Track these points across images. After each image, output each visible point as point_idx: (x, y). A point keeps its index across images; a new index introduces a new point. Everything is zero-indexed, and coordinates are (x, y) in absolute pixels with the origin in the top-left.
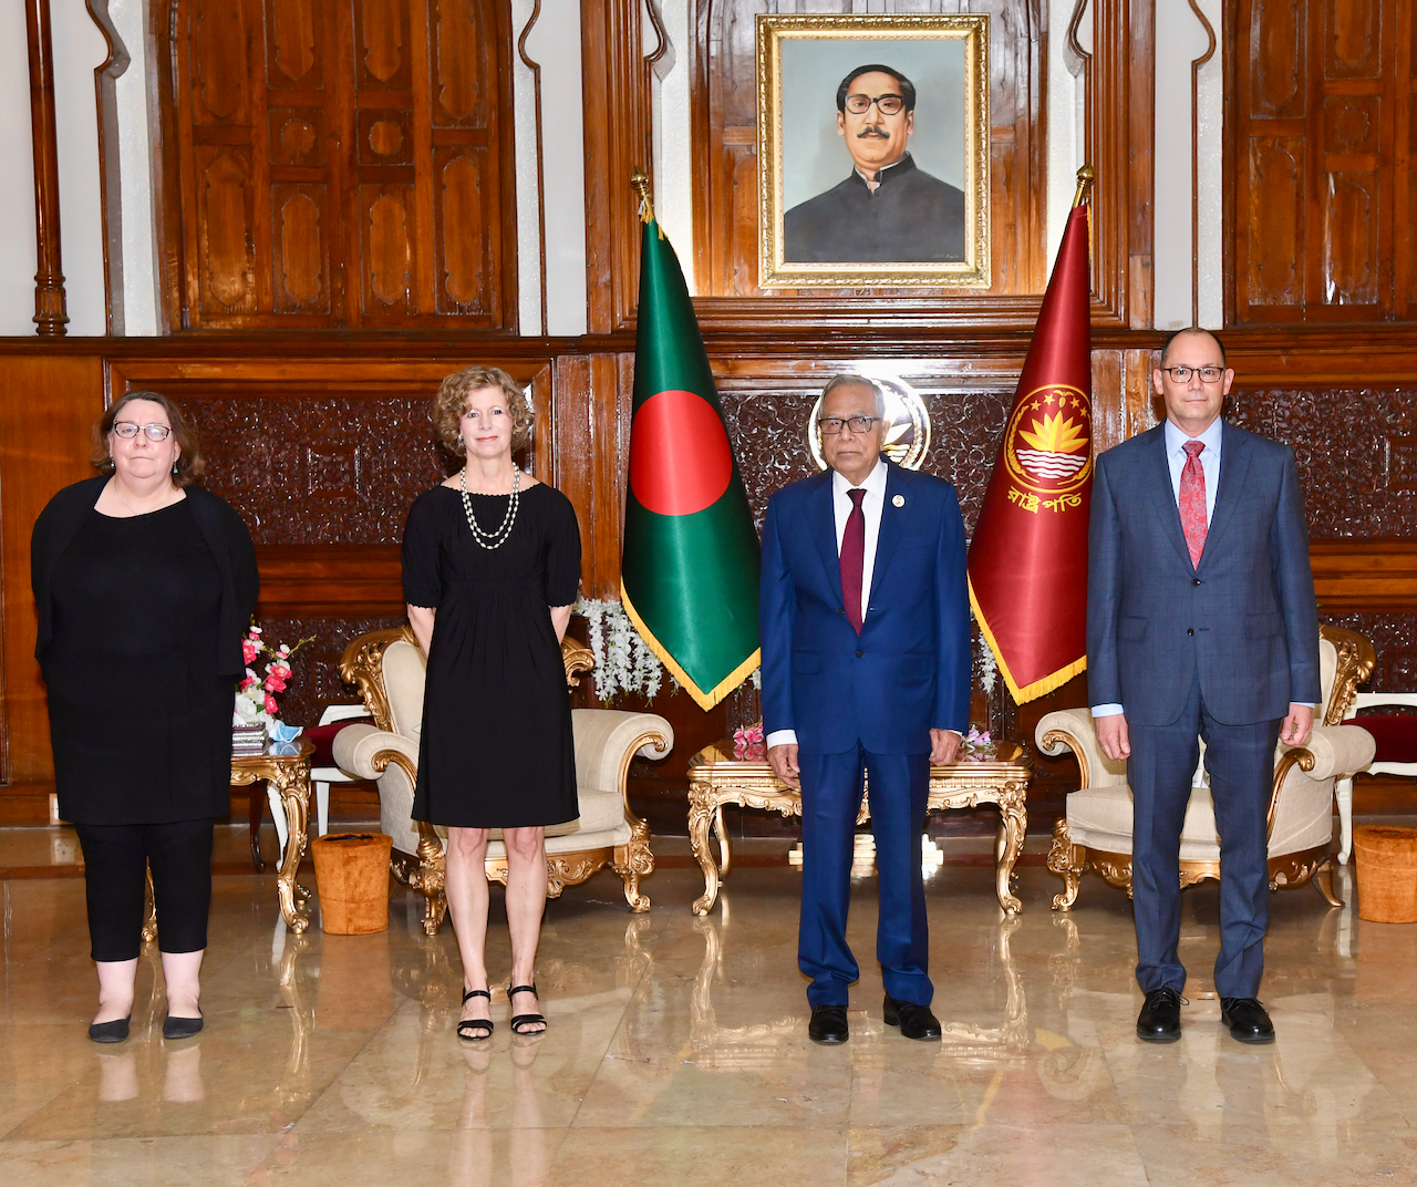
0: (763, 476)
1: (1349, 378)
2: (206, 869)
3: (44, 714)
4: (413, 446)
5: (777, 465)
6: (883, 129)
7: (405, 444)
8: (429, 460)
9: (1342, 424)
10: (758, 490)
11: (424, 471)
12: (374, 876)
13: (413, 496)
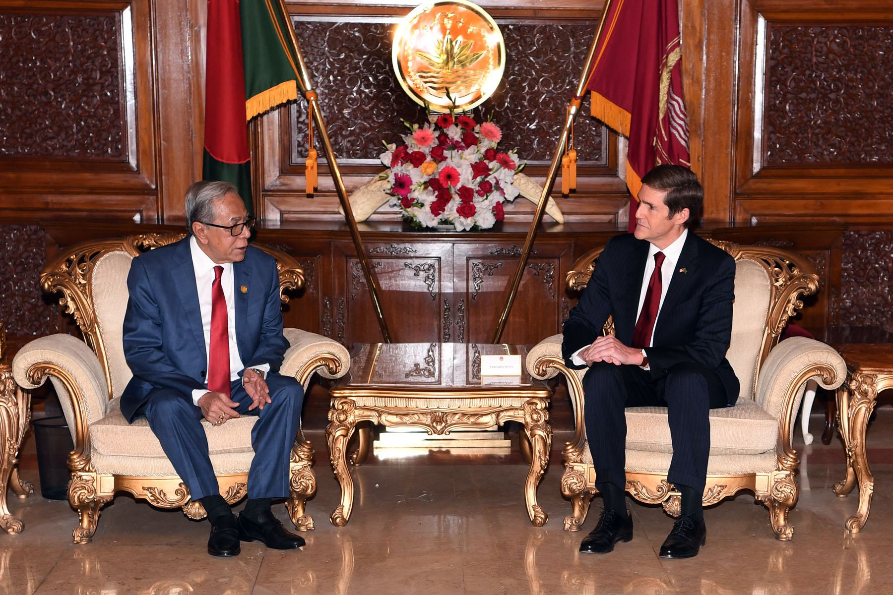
0: (350, 99)
1: (881, 16)
2: (467, 336)
3: (216, 474)
4: (18, 62)
5: (363, 88)
7: (10, 59)
8: (34, 75)
9: (873, 58)
10: (346, 111)
11: (30, 86)
12: (309, 162)
13: (20, 110)
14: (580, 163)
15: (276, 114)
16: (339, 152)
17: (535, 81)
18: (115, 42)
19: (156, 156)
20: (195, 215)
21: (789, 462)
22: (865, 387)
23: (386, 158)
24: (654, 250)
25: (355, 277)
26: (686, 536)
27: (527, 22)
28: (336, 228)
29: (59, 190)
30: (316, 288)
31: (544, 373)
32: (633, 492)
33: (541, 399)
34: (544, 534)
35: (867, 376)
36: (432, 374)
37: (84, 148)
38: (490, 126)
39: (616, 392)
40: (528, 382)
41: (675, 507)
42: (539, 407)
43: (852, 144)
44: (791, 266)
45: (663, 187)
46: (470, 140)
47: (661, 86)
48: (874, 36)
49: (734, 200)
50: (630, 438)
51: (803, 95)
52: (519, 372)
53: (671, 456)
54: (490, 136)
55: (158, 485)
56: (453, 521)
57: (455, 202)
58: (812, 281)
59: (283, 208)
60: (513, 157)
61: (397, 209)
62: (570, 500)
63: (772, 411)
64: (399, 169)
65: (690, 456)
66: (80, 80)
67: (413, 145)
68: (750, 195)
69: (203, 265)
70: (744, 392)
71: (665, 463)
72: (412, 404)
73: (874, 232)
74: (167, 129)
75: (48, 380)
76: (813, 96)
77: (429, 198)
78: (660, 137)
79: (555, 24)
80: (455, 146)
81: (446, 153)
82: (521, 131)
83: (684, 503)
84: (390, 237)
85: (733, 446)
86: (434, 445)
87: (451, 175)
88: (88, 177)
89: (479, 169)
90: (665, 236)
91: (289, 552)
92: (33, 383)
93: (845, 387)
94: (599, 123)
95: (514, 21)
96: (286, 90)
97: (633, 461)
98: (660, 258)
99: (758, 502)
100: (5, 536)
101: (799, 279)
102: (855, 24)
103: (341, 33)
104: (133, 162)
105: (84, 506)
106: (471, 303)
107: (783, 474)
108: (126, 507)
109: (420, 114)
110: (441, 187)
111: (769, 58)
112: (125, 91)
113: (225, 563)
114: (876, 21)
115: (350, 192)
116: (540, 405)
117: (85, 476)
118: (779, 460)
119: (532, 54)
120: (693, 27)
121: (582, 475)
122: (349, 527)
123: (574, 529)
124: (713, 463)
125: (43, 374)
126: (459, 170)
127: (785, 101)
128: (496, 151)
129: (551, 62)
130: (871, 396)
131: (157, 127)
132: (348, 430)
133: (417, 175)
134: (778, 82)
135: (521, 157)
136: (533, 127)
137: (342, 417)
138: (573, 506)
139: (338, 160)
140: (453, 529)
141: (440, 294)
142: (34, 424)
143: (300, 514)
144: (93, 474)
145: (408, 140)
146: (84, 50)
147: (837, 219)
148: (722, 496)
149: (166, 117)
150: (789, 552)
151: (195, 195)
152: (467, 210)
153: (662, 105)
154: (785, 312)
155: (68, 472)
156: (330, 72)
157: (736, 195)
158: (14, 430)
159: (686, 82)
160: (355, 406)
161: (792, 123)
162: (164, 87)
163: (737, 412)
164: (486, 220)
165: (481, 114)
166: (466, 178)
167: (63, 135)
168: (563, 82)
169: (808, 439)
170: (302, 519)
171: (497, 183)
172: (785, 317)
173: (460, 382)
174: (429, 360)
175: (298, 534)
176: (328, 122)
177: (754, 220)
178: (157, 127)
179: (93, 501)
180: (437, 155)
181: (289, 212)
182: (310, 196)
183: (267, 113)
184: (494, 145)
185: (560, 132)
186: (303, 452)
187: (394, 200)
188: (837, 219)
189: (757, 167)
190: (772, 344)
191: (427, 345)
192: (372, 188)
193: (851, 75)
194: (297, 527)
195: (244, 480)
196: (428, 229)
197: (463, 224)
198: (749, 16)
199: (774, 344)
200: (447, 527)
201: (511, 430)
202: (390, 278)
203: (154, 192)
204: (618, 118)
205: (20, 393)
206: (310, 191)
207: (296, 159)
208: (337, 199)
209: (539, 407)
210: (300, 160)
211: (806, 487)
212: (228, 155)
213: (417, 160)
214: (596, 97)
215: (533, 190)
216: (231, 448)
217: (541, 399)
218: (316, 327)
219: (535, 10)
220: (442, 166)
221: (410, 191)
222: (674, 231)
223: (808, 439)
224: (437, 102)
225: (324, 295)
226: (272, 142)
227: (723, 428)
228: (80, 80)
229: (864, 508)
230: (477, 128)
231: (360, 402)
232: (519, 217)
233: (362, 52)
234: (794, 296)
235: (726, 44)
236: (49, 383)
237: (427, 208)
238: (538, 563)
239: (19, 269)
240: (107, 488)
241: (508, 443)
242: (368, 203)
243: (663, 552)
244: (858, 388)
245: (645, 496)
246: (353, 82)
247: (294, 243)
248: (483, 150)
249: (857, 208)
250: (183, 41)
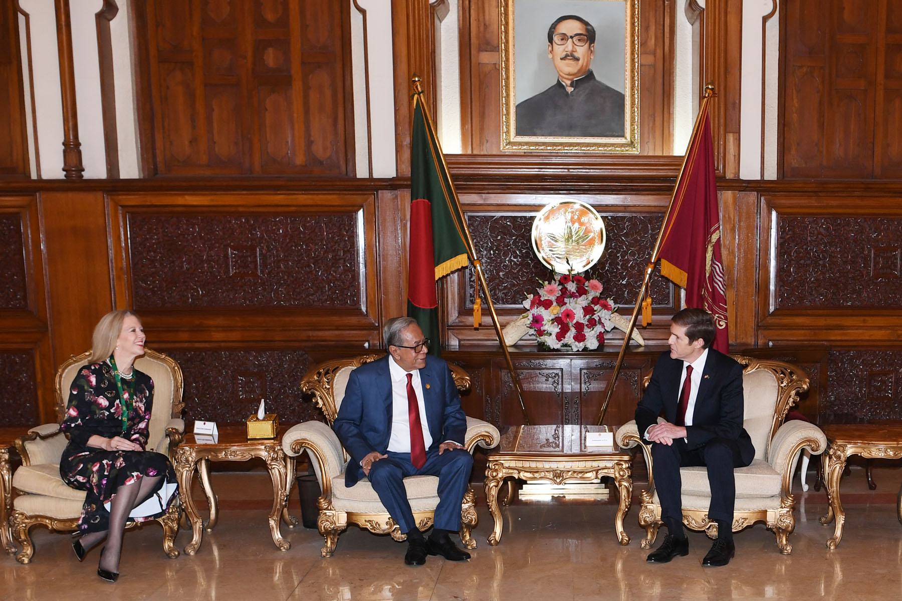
6: (576, 54)
12: (475, 307)
14: (655, 306)
15: (456, 275)
16: (496, 300)
17: (626, 253)
18: (353, 232)
19: (378, 304)
20: (391, 341)
21: (789, 502)
22: (839, 453)
23: (527, 304)
24: (686, 364)
25: (506, 382)
26: (722, 549)
27: (620, 214)
28: (494, 350)
29: (315, 328)
30: (481, 389)
31: (628, 444)
32: (686, 522)
33: (626, 461)
34: (628, 550)
35: (840, 446)
36: (558, 446)
37: (332, 300)
38: (595, 282)
39: (684, 454)
40: (619, 451)
41: (714, 533)
42: (624, 466)
43: (834, 293)
44: (791, 373)
45: (685, 324)
46: (581, 291)
47: (707, 255)
48: (848, 224)
49: (757, 331)
50: (684, 487)
51: (802, 262)
52: (611, 443)
53: (710, 499)
54: (595, 288)
55: (375, 519)
56: (572, 542)
57: (572, 332)
58: (805, 383)
59: (460, 337)
60: (611, 302)
61: (534, 337)
62: (645, 528)
63: (778, 470)
64: (536, 311)
65: (723, 499)
67: (544, 294)
68: (767, 327)
69: (397, 373)
70: (759, 455)
71: (706, 503)
72: (540, 465)
73: (849, 351)
74: (386, 288)
75: (305, 451)
76: (809, 262)
77: (555, 329)
78: (708, 290)
79: (638, 215)
80: (572, 295)
81: (566, 300)
82: (616, 285)
83: (720, 529)
84: (529, 356)
86: (557, 493)
87: (569, 315)
88: (335, 319)
89: (588, 310)
90: (693, 355)
91: (460, 563)
92: (295, 452)
93: (826, 453)
94: (667, 280)
95: (611, 214)
96: (462, 260)
97: (686, 502)
98: (690, 369)
99: (768, 529)
100: (279, 552)
101: (796, 382)
102: (835, 216)
103: (498, 223)
104: (364, 309)
105: (328, 533)
106: (582, 398)
107: (785, 510)
108: (354, 534)
109: (548, 274)
110: (563, 322)
111: (779, 238)
112: (358, 263)
113: (416, 571)
114: (849, 214)
115: (503, 326)
116: (625, 466)
117: (328, 513)
118: (782, 501)
119: (624, 235)
120: (729, 217)
121: (652, 511)
122: (498, 546)
123: (648, 547)
124: (738, 503)
125: (301, 447)
126: (574, 311)
127: (789, 266)
128: (600, 298)
129: (636, 241)
130: (843, 459)
131: (379, 286)
132: (498, 483)
133: (547, 315)
134: (785, 253)
135: (615, 303)
136: (624, 282)
137: (494, 474)
138: (647, 532)
139: (496, 306)
140: (572, 549)
141: (562, 392)
142: (297, 480)
143: (468, 537)
144: (334, 512)
145: (541, 292)
146: (333, 237)
147: (825, 343)
148: (745, 525)
149: (385, 279)
150: (789, 562)
151: (389, 328)
152: (580, 337)
153: (708, 267)
154: (787, 403)
155: (317, 510)
156: (491, 248)
157: (758, 327)
158: (284, 483)
159: (724, 252)
160: (505, 466)
161: (794, 281)
162: (384, 260)
163: (754, 470)
164: (592, 343)
165: (588, 275)
166: (579, 316)
167: (319, 292)
168: (644, 254)
169: (806, 488)
170: (469, 540)
171: (600, 319)
172: (788, 407)
173: (576, 450)
174: (556, 436)
175: (466, 551)
176: (490, 281)
177: (771, 344)
178: (379, 286)
179: (333, 529)
180: (561, 302)
181: (464, 340)
182: (476, 329)
183: (448, 275)
184: (598, 295)
185: (640, 286)
186: (469, 497)
187: (532, 331)
188: (825, 343)
189: (772, 309)
190: (778, 425)
191: (554, 427)
192: (518, 323)
193: (833, 249)
194: (466, 546)
195: (431, 515)
196: (554, 350)
197: (578, 346)
198: (766, 210)
199: (781, 425)
200: (568, 548)
201: (606, 481)
202: (529, 382)
203: (377, 328)
204: (678, 276)
205: (289, 460)
206: (476, 326)
207: (468, 305)
208: (494, 331)
209: (624, 466)
210: (471, 306)
211: (804, 519)
212: (424, 303)
213: (547, 304)
214: (664, 262)
215: (625, 324)
216: (423, 495)
217: (626, 461)
218: (482, 417)
219: (626, 206)
220: (564, 308)
221: (542, 325)
222: (695, 354)
223: (806, 488)
224: (561, 268)
225: (486, 394)
226: (453, 295)
227: (743, 480)
229: (838, 533)
230: (587, 284)
231: (506, 464)
232: (615, 343)
233: (512, 235)
234: (793, 392)
235: (750, 228)
236: (305, 452)
237: (554, 336)
238: (624, 569)
239: (292, 379)
240: (342, 521)
241: (607, 491)
242: (515, 333)
243: (705, 562)
244: (835, 453)
245: (694, 525)
246: (506, 255)
247: (467, 360)
248: (590, 298)
249: (836, 336)
250: (396, 230)
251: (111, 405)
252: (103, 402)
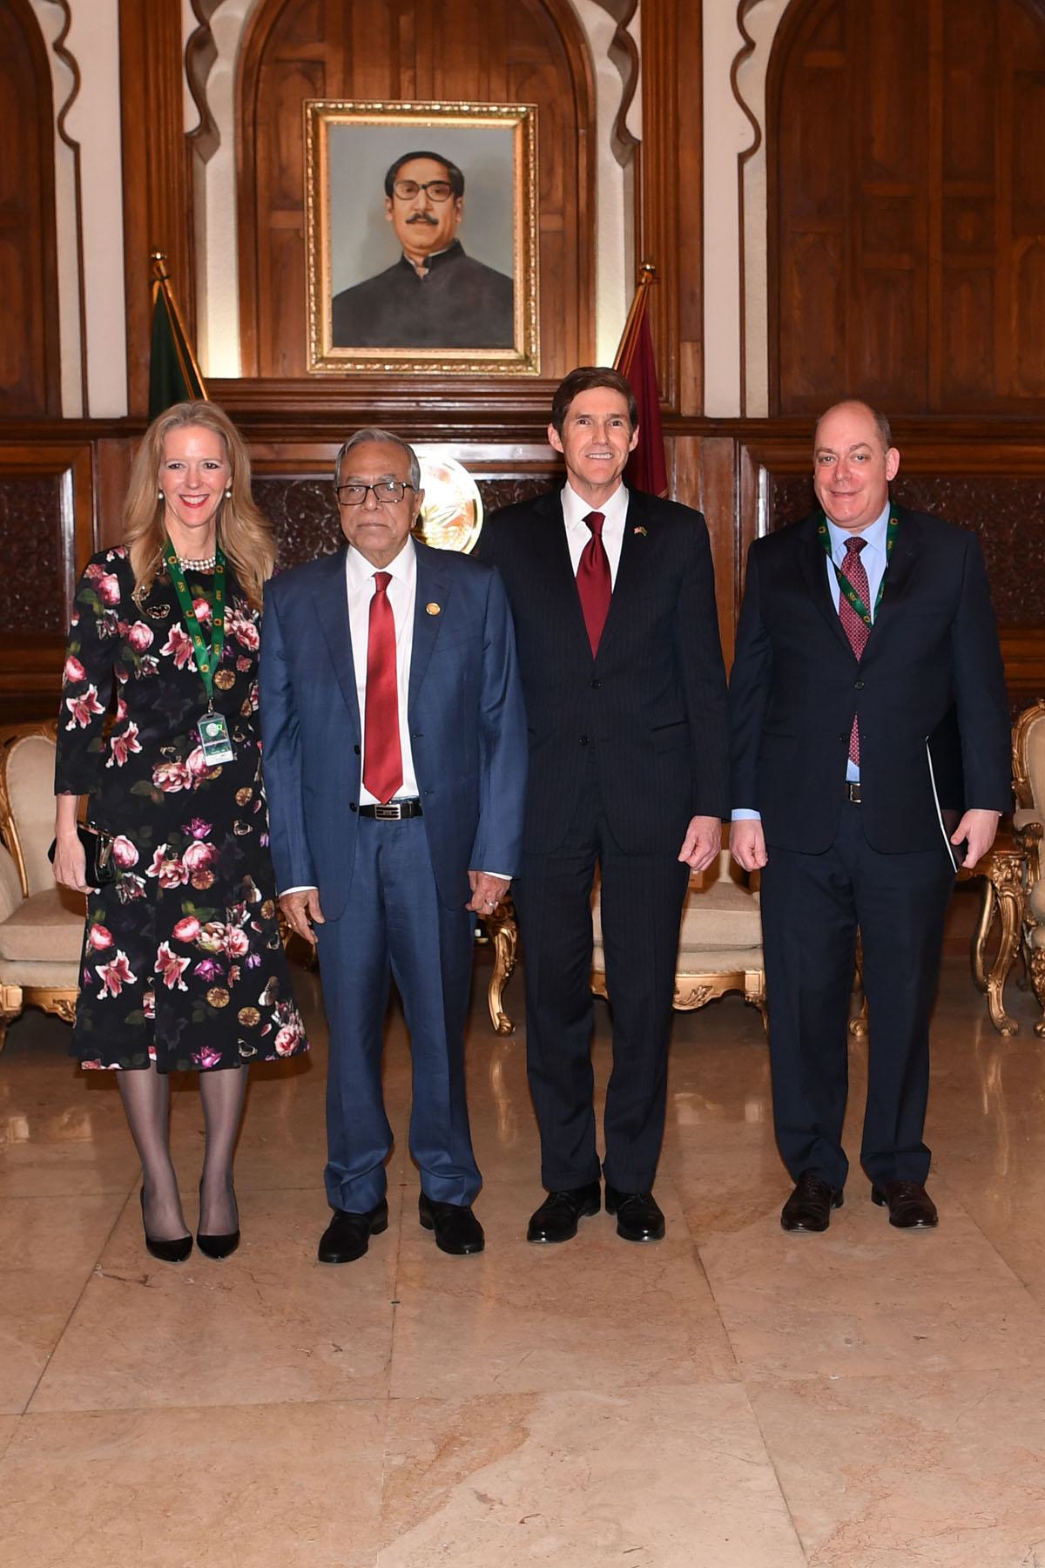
66: (15, 549)
85: (717, 941)
124: (684, 961)
148: (708, 998)
198: (749, 468)
228: (15, 549)
251: (160, 639)
252: (143, 635)
